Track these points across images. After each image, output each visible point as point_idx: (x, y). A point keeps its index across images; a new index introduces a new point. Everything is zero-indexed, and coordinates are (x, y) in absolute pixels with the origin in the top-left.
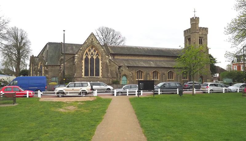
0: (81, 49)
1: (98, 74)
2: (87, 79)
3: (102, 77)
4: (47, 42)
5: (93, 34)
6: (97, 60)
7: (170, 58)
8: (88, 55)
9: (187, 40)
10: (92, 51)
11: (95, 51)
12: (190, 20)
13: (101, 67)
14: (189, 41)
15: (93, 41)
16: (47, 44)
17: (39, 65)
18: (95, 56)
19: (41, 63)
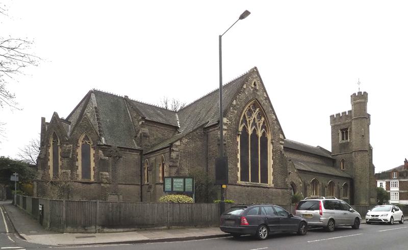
0: (235, 106)
1: (265, 180)
2: (247, 188)
3: (272, 185)
4: (91, 89)
5: (257, 72)
6: (264, 140)
7: (308, 158)
8: (256, 127)
9: (340, 131)
10: (255, 115)
11: (259, 117)
12: (350, 98)
13: (272, 161)
14: (343, 133)
15: (257, 90)
16: (91, 92)
17: (80, 143)
18: (259, 130)
19: (86, 138)
